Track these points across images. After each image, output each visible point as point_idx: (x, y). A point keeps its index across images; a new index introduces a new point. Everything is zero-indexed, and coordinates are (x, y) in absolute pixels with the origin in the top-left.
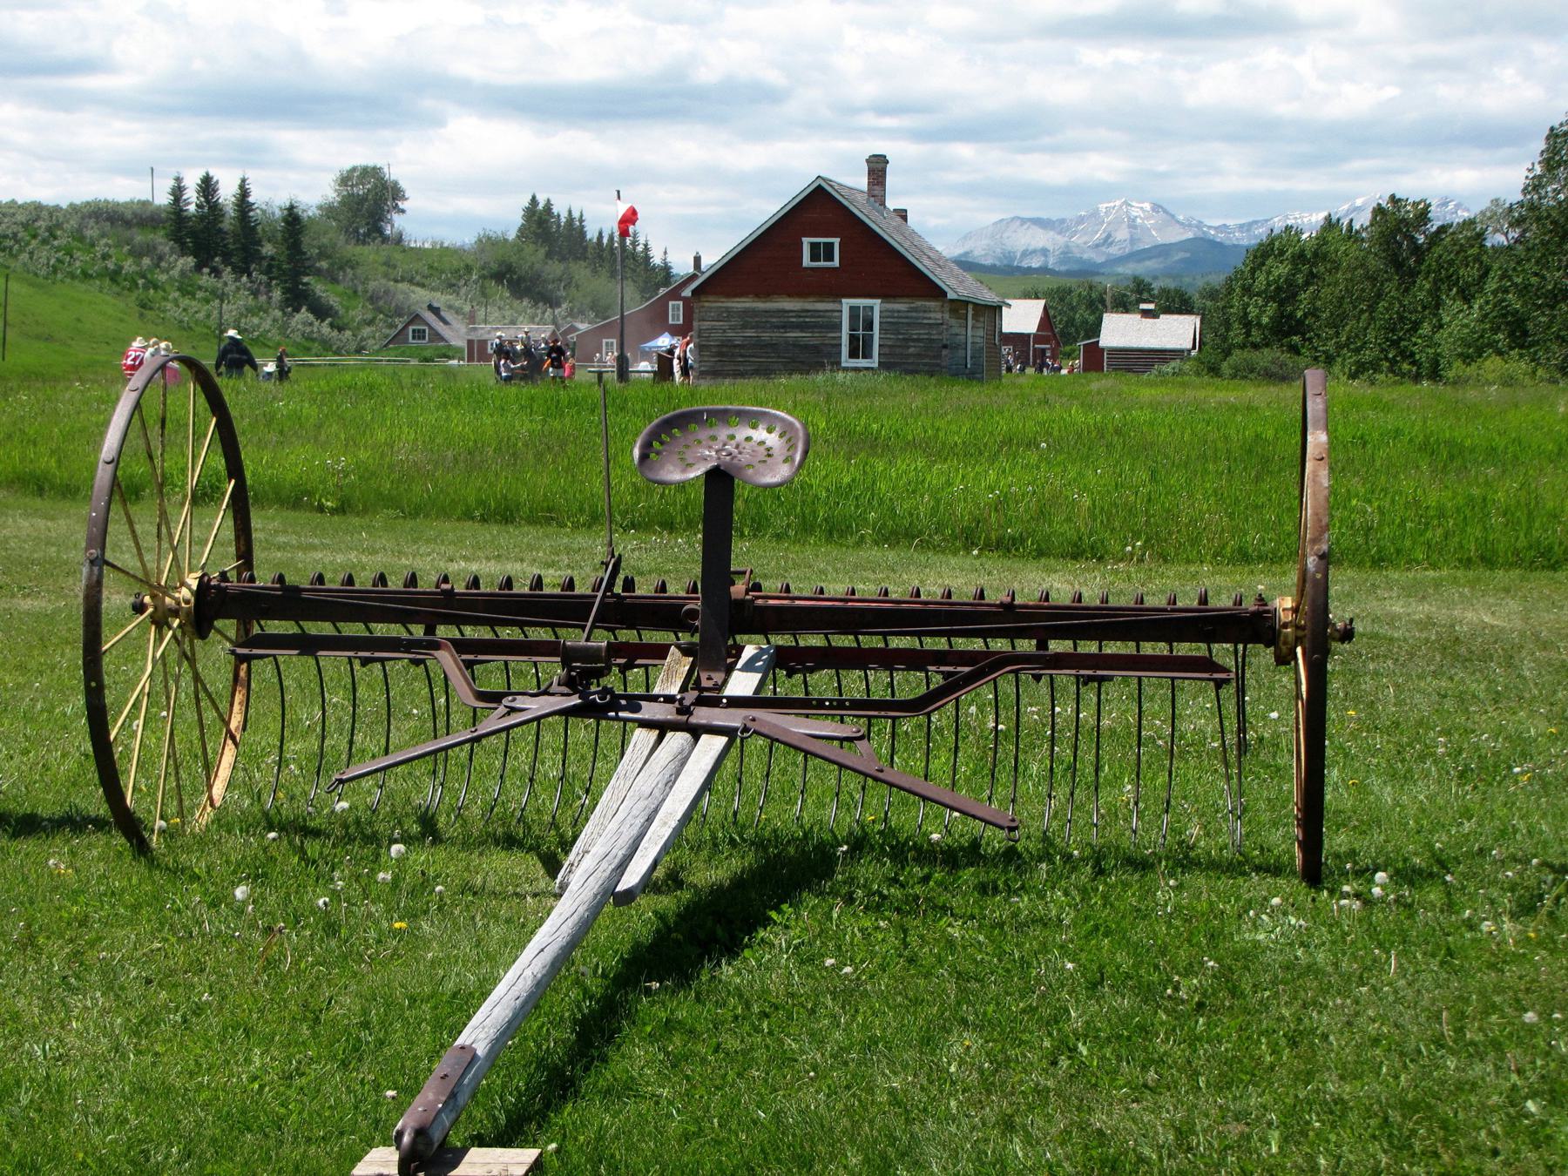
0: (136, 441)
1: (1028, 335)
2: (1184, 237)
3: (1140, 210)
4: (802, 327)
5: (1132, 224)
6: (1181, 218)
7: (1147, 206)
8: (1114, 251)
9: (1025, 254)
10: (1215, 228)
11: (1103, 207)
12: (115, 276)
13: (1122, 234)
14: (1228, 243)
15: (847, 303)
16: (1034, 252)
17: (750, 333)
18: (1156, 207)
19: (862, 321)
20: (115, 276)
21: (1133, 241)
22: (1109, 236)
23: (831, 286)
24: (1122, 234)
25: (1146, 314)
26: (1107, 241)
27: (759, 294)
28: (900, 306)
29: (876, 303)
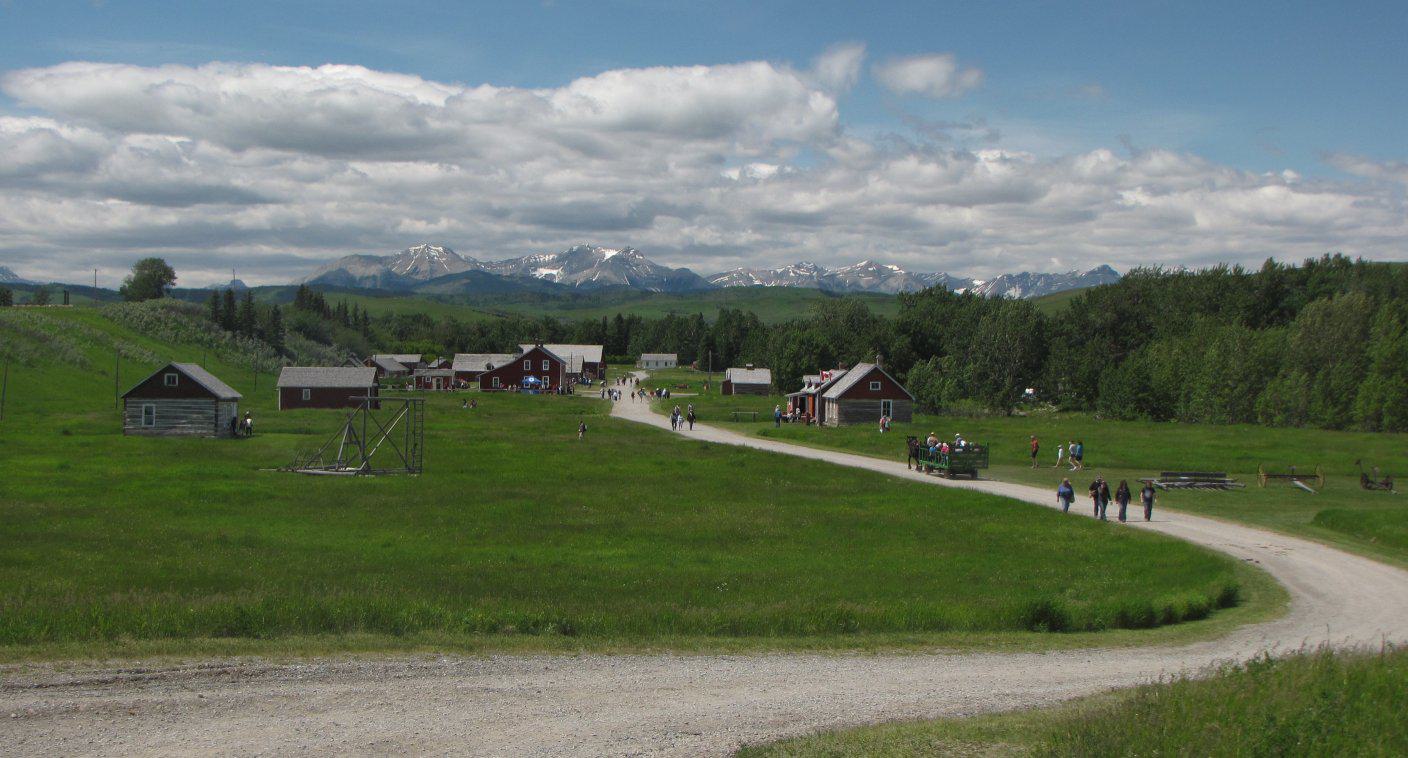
0: (1310, 481)
1: (597, 364)
2: (464, 270)
3: (436, 251)
4: (869, 407)
5: (431, 260)
6: (463, 257)
7: (441, 249)
8: (419, 277)
9: (362, 279)
10: (484, 264)
11: (412, 249)
12: (199, 341)
13: (425, 267)
14: (493, 273)
15: (883, 400)
16: (368, 278)
17: (854, 409)
18: (446, 250)
19: (887, 405)
20: (199, 341)
21: (432, 271)
22: (416, 268)
23: (878, 396)
24: (425, 267)
25: (749, 368)
26: (415, 270)
27: (857, 398)
28: (898, 401)
29: (891, 401)
